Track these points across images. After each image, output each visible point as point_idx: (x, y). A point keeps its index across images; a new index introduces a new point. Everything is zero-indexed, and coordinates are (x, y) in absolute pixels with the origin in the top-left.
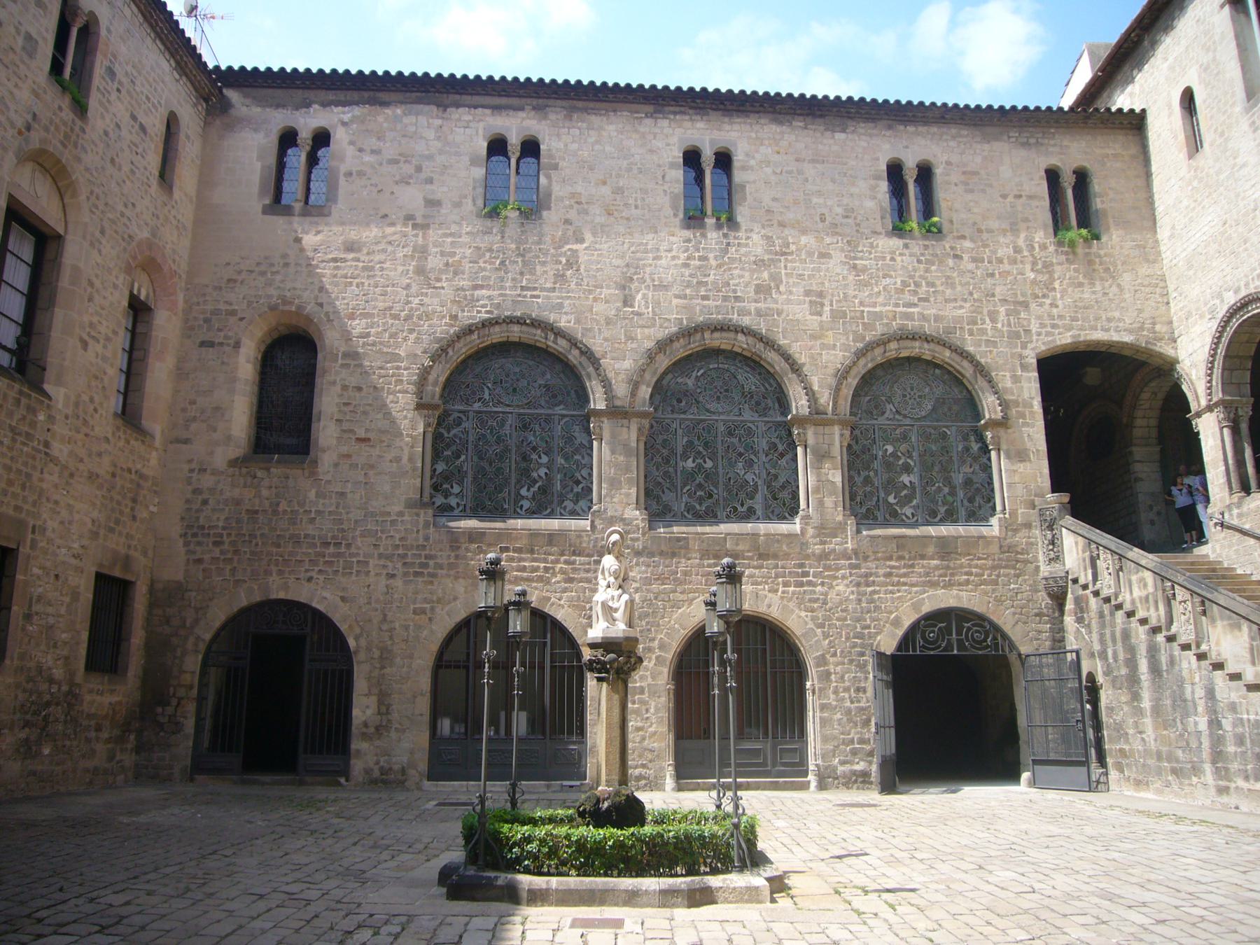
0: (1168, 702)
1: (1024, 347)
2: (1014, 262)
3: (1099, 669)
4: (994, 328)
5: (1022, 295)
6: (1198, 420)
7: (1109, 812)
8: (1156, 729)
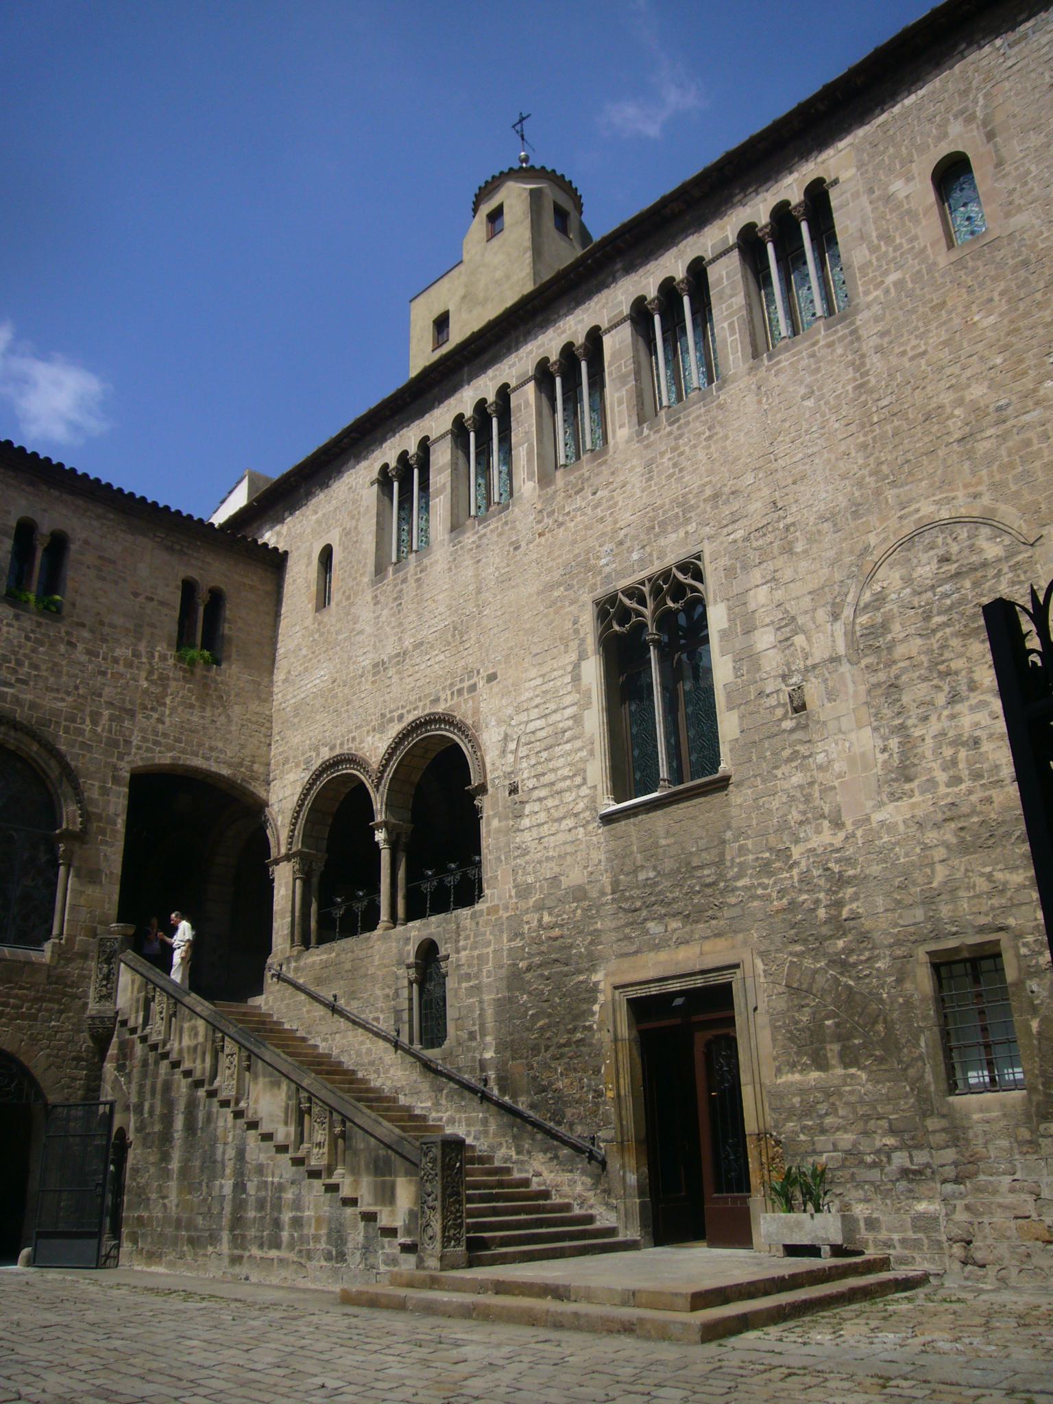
0: (198, 1163)
1: (121, 758)
2: (130, 665)
3: (132, 1124)
4: (94, 732)
5: (131, 702)
6: (276, 868)
7: (115, 1292)
8: (180, 1192)
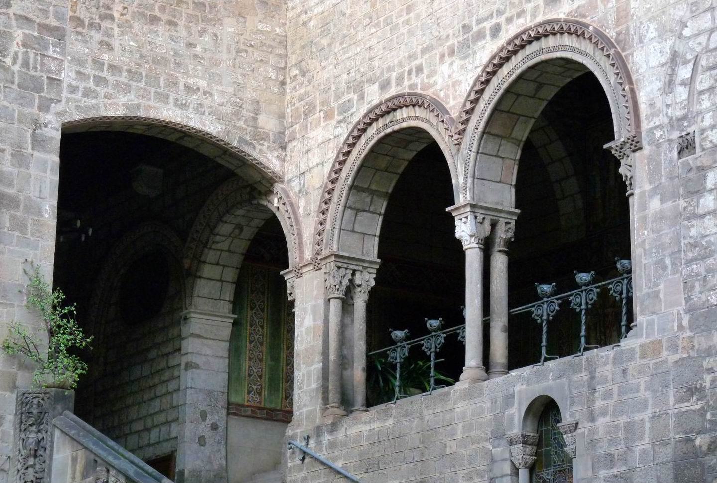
1: (44, 107)
